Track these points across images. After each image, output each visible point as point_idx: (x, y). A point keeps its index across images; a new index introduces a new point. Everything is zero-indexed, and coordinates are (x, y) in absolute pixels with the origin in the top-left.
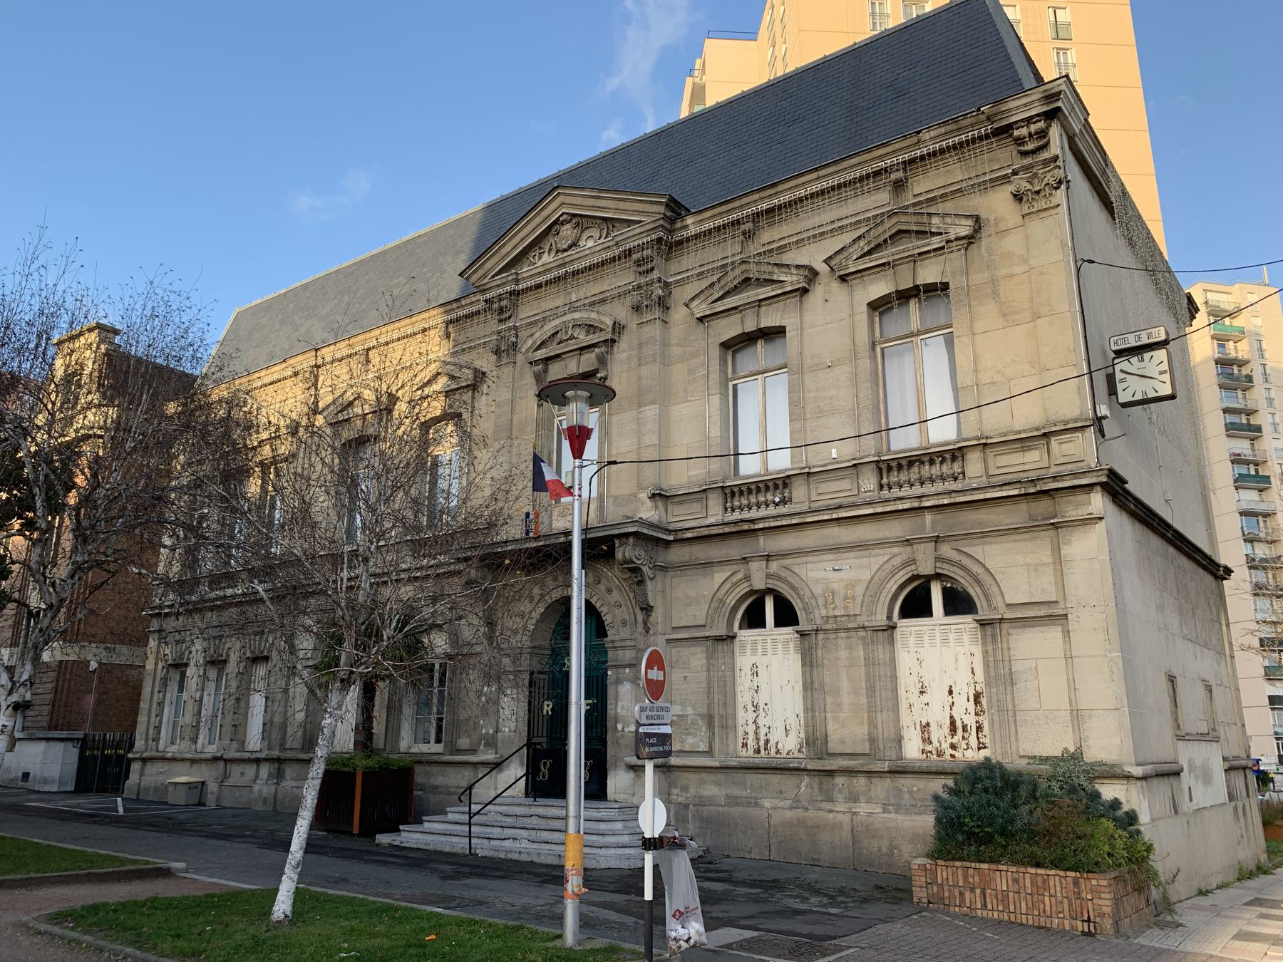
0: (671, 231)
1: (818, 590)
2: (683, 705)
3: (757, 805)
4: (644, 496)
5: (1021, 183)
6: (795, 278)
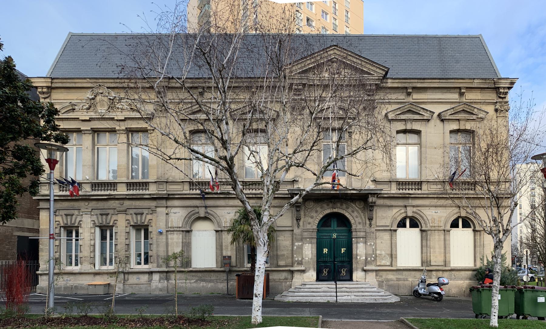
0: (382, 82)
1: (429, 218)
2: (381, 250)
3: (407, 280)
5: (498, 106)
6: (428, 115)
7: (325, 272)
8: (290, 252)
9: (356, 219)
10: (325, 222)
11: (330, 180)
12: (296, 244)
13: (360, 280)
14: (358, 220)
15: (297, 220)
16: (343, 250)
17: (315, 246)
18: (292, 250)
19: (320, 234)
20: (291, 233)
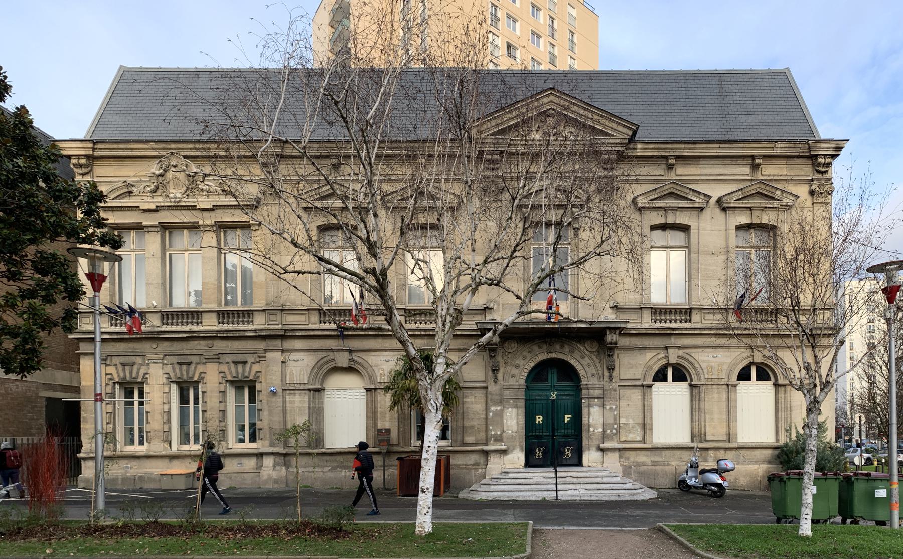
1: (704, 366)
2: (627, 418)
3: (668, 464)
4: (607, 306)
6: (701, 201)
7: (539, 453)
8: (483, 422)
9: (587, 369)
10: (538, 374)
11: (544, 307)
12: (492, 409)
13: (594, 464)
14: (591, 370)
15: (493, 371)
16: (567, 418)
17: (522, 412)
18: (487, 418)
19: (531, 393)
20: (484, 391)
